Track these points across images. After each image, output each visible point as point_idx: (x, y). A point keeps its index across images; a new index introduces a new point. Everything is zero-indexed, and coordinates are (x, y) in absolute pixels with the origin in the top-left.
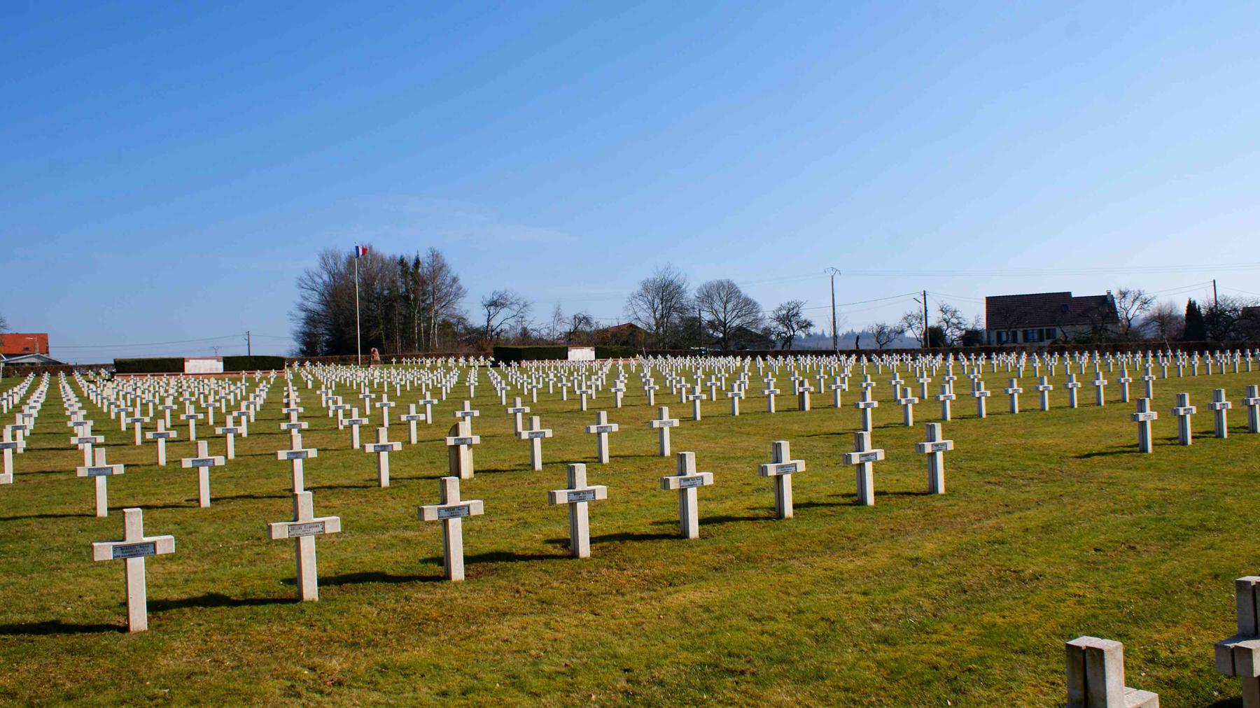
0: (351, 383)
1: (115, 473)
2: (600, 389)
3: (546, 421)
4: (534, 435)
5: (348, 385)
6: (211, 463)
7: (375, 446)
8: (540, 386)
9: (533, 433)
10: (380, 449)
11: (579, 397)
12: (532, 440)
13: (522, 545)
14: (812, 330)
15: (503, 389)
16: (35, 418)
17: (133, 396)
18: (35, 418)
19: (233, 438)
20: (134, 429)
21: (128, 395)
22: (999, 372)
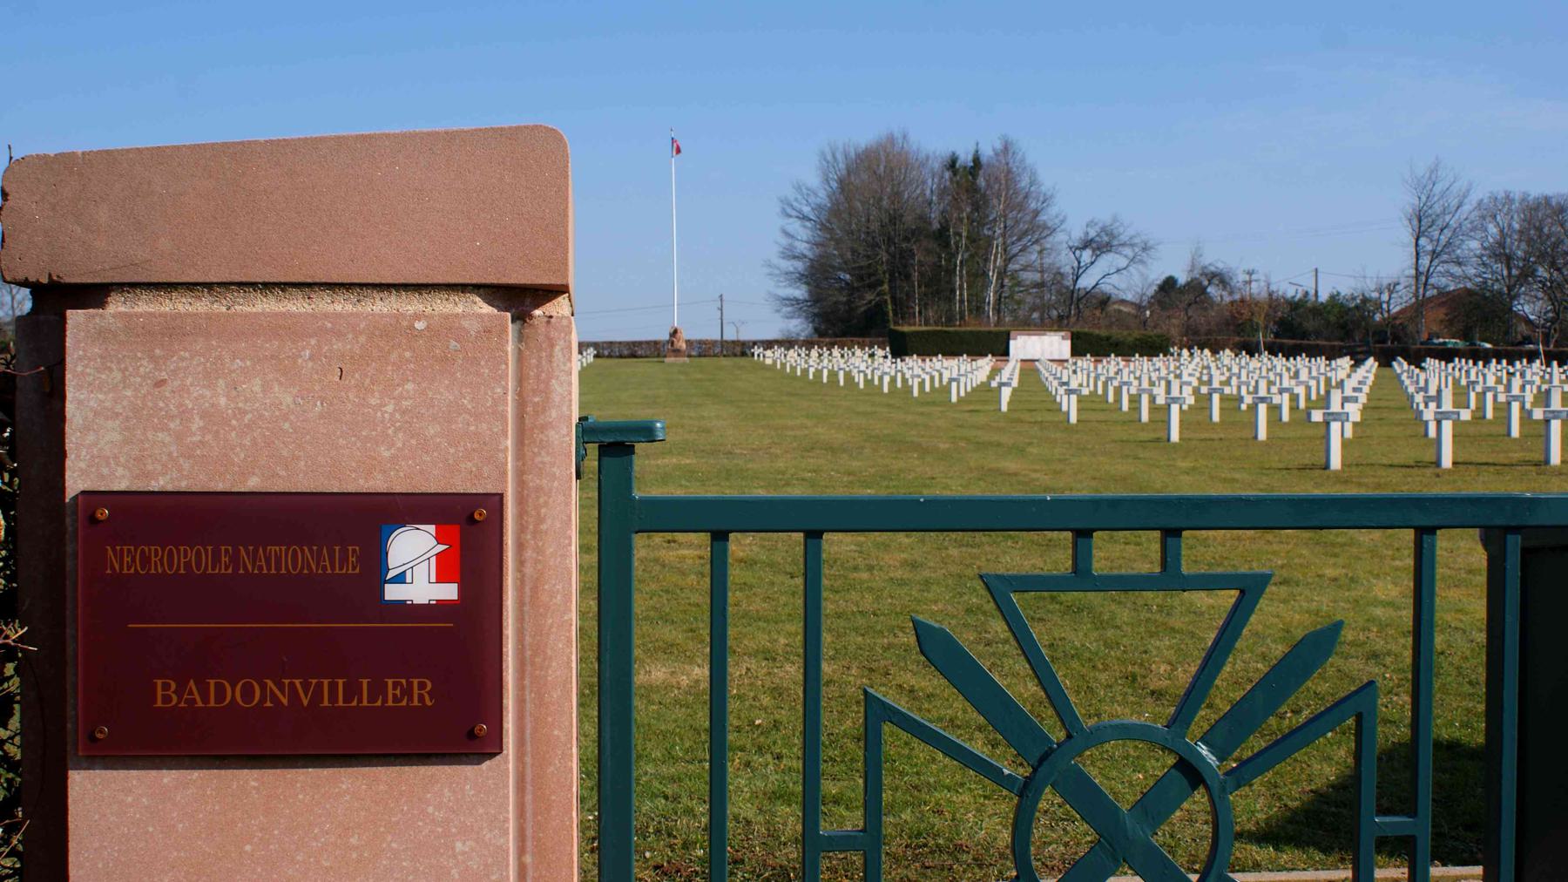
0: (1135, 400)
1: (1358, 419)
2: (1286, 417)
3: (1402, 409)
4: (1331, 417)
5: (1125, 406)
6: (1455, 416)
7: (1324, 414)
8: (1466, 415)
9: (1329, 414)
10: (1551, 415)
11: (1305, 416)
12: (1509, 403)
13: (903, 491)
14: (1425, 410)
15: (1446, 415)
16: (1355, 424)
17: (1133, 391)
18: (1355, 424)
19: (1265, 410)
20: (1140, 402)
21: (1125, 388)
22: (1292, 421)
